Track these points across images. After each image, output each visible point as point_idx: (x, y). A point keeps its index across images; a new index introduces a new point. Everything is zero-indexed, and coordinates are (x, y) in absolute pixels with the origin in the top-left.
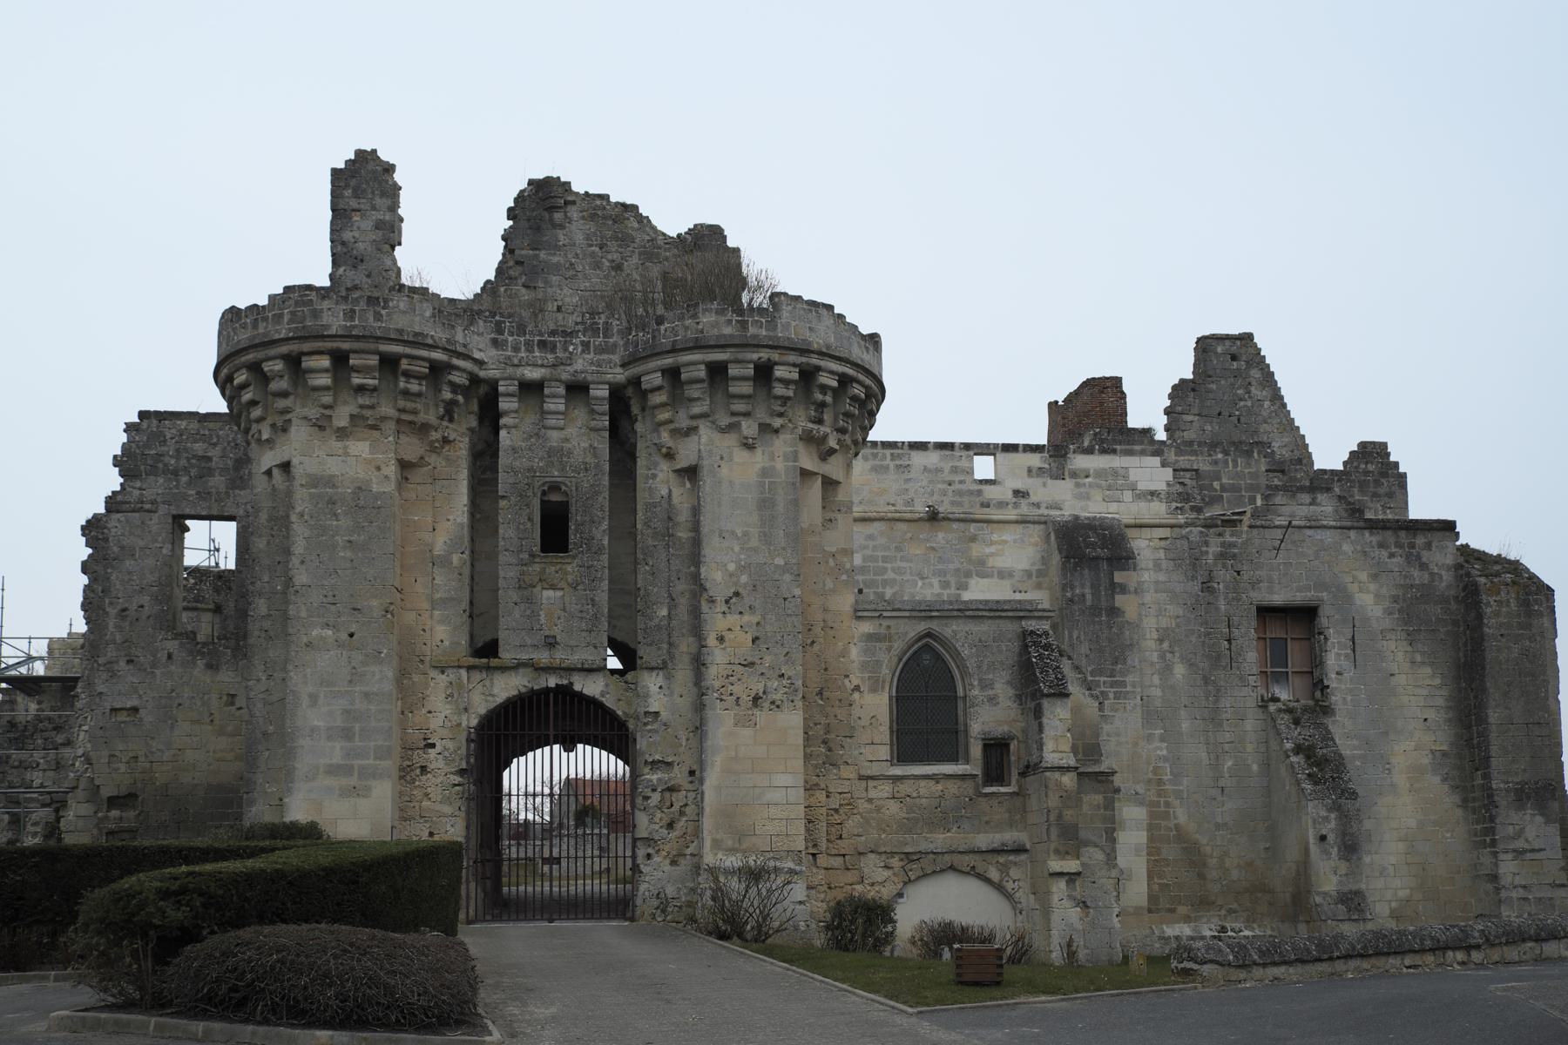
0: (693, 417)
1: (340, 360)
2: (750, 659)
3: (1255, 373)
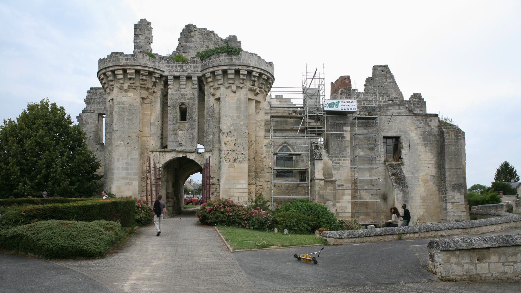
1: (125, 71)
3: (388, 75)
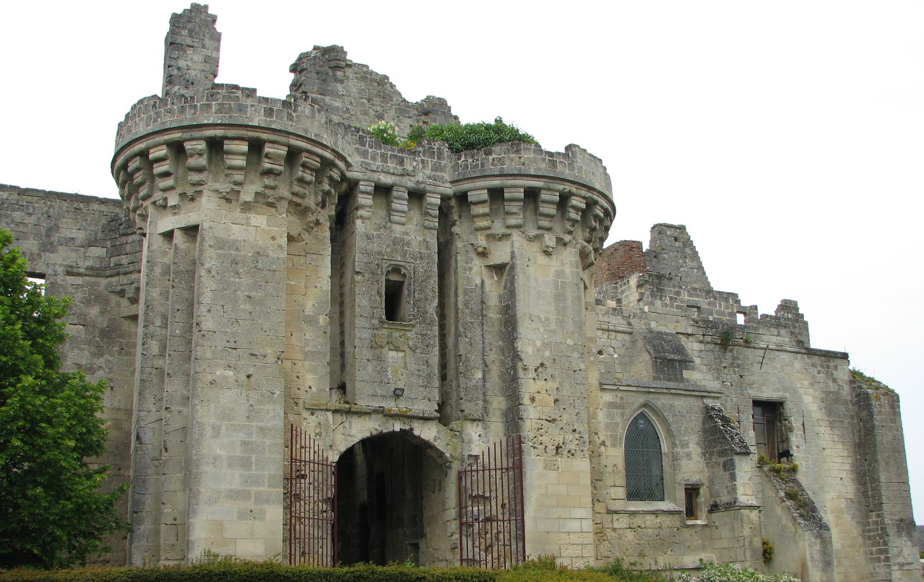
0: (508, 227)
1: (256, 147)
2: (553, 417)
3: (688, 250)
